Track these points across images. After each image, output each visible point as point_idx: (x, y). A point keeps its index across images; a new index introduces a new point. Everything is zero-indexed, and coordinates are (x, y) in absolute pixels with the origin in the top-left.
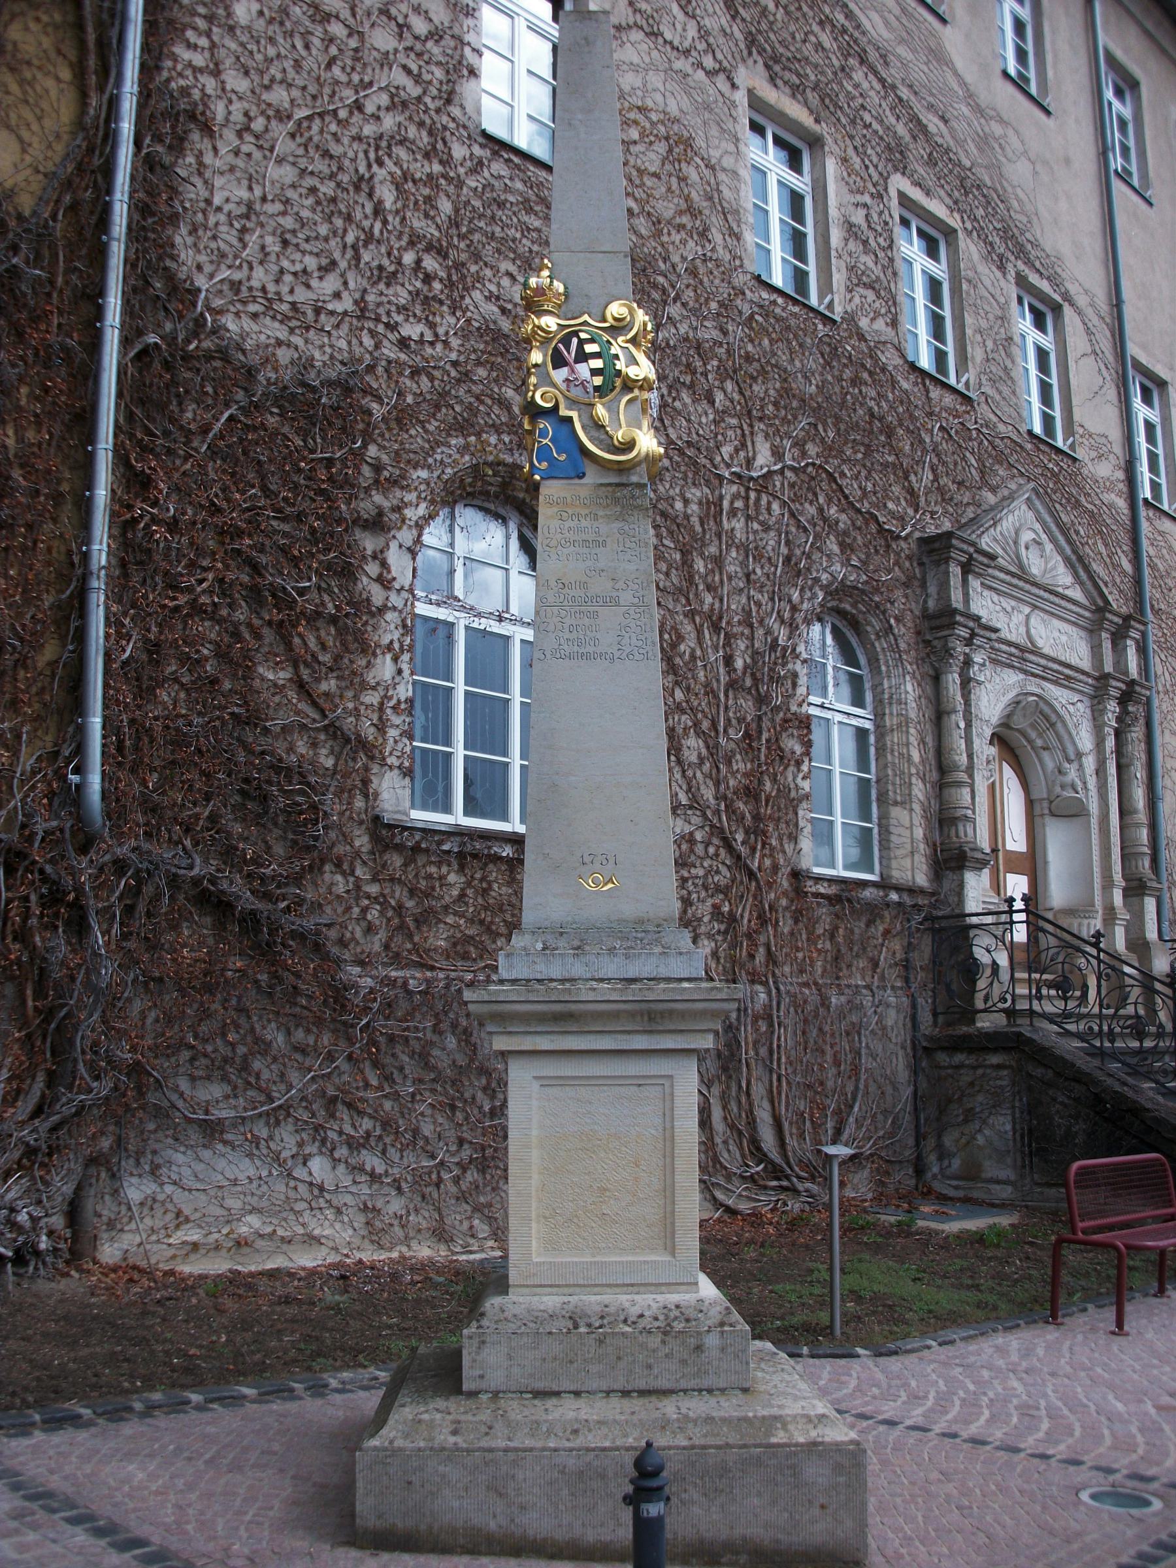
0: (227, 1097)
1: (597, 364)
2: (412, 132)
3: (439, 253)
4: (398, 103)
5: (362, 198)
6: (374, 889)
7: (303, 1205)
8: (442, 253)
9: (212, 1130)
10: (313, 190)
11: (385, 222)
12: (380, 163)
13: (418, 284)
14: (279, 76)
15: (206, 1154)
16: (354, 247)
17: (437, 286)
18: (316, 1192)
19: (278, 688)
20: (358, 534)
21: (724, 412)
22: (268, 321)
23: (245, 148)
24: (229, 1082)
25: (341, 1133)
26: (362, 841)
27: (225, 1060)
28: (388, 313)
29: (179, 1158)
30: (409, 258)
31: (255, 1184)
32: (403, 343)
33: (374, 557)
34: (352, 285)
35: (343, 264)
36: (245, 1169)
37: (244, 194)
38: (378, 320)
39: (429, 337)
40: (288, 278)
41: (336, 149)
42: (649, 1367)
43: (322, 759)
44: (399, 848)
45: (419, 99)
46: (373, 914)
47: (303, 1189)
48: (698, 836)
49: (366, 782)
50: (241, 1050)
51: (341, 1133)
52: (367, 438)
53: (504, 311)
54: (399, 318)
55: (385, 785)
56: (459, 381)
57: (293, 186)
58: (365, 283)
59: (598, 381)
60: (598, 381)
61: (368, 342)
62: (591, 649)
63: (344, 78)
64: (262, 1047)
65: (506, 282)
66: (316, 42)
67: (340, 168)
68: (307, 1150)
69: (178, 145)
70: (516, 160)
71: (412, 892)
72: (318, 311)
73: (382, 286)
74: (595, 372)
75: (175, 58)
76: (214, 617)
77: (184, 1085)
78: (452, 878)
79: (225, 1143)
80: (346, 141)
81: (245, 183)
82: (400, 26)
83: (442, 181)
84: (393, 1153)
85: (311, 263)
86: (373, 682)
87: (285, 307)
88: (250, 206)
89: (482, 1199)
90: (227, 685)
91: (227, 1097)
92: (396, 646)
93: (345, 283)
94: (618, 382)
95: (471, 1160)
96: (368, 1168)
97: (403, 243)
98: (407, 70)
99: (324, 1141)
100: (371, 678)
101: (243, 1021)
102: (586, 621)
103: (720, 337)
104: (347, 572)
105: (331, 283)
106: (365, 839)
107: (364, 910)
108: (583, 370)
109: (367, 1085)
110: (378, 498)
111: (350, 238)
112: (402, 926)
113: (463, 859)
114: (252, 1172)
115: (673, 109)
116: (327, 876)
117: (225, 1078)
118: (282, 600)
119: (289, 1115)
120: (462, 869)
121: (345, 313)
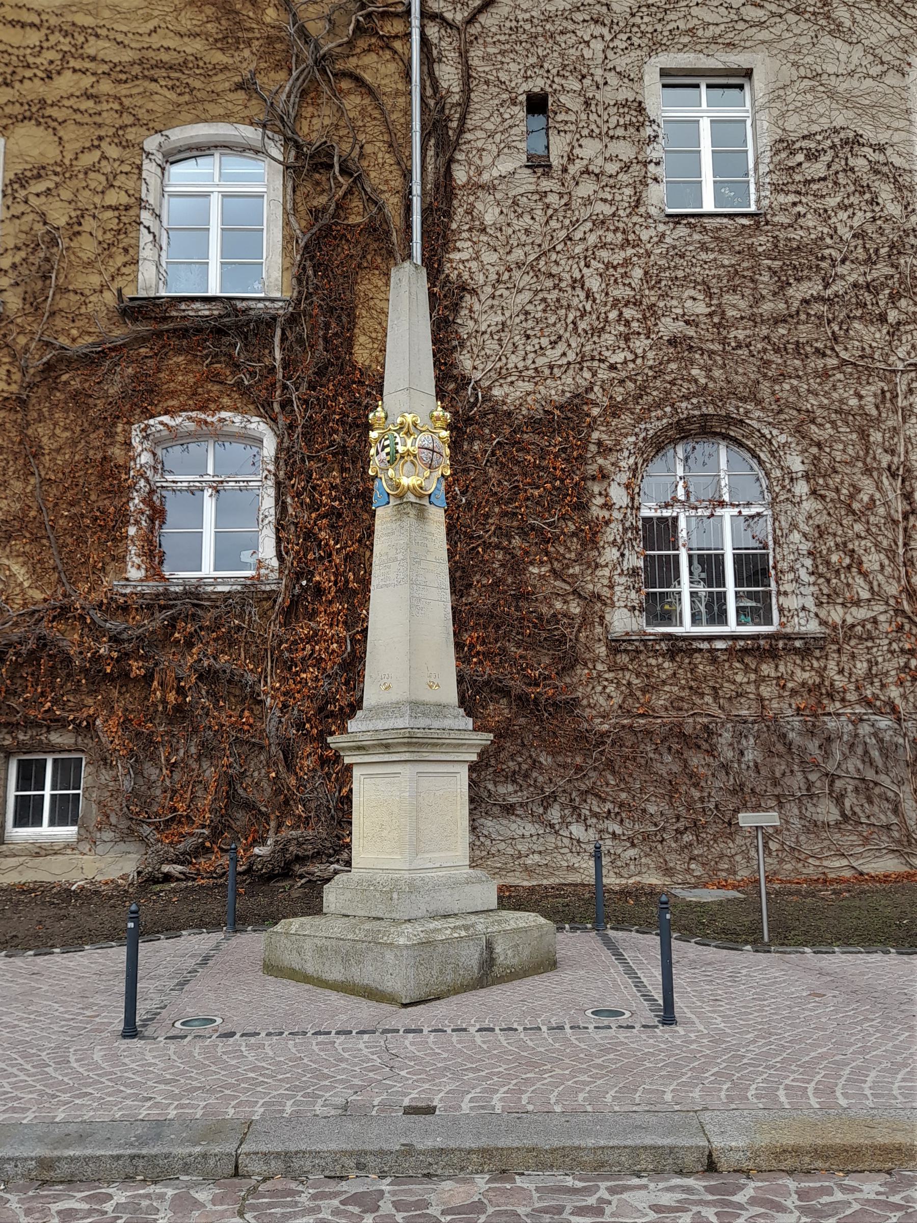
0: (516, 792)
2: (610, 237)
3: (635, 304)
4: (600, 223)
5: (578, 291)
6: (610, 675)
7: (566, 850)
8: (637, 304)
9: (509, 810)
10: (544, 300)
11: (594, 300)
12: (587, 266)
13: (622, 328)
14: (515, 244)
15: (505, 822)
16: (574, 323)
17: (635, 324)
18: (575, 842)
19: (542, 577)
20: (589, 483)
21: (899, 323)
22: (520, 383)
23: (498, 293)
24: (517, 783)
25: (590, 810)
26: (602, 650)
27: (514, 772)
28: (600, 354)
29: (489, 824)
30: (613, 315)
31: (535, 838)
32: (613, 367)
33: (600, 494)
34: (574, 345)
35: (567, 335)
36: (531, 829)
37: (500, 318)
38: (593, 359)
39: (630, 357)
40: (531, 356)
41: (555, 270)
42: (528, 337)
43: (572, 610)
44: (626, 651)
45: (614, 215)
46: (611, 689)
47: (566, 841)
48: (882, 618)
49: (602, 618)
50: (524, 767)
51: (590, 810)
52: (591, 428)
53: (687, 322)
54: (607, 354)
55: (615, 618)
56: (655, 378)
57: (530, 302)
58: (583, 340)
59: (388, 458)
60: (388, 458)
61: (587, 375)
63: (559, 225)
64: (535, 764)
65: (689, 303)
66: (539, 212)
67: (560, 280)
68: (569, 819)
69: (456, 308)
70: (692, 221)
71: (638, 675)
72: (551, 367)
73: (595, 339)
74: (388, 454)
75: (451, 261)
76: (498, 546)
77: (490, 786)
78: (666, 665)
79: (517, 815)
80: (563, 262)
81: (499, 312)
82: (597, 175)
83: (635, 259)
84: (627, 822)
85: (545, 342)
86: (604, 563)
87: (531, 373)
88: (503, 324)
89: (696, 852)
90: (510, 580)
91: (516, 792)
92: (619, 541)
93: (569, 345)
94: (398, 456)
95: (686, 829)
96: (610, 830)
97: (608, 308)
98: (604, 201)
99: (579, 815)
100: (602, 561)
101: (524, 751)
103: (891, 271)
104: (582, 507)
105: (561, 347)
106: (604, 648)
107: (605, 687)
109: (607, 784)
110: (600, 461)
111: (571, 317)
112: (631, 694)
113: (672, 654)
114: (533, 831)
115: (839, 122)
116: (579, 672)
117: (514, 782)
118: (539, 531)
119: (555, 800)
120: (672, 659)
121: (569, 363)
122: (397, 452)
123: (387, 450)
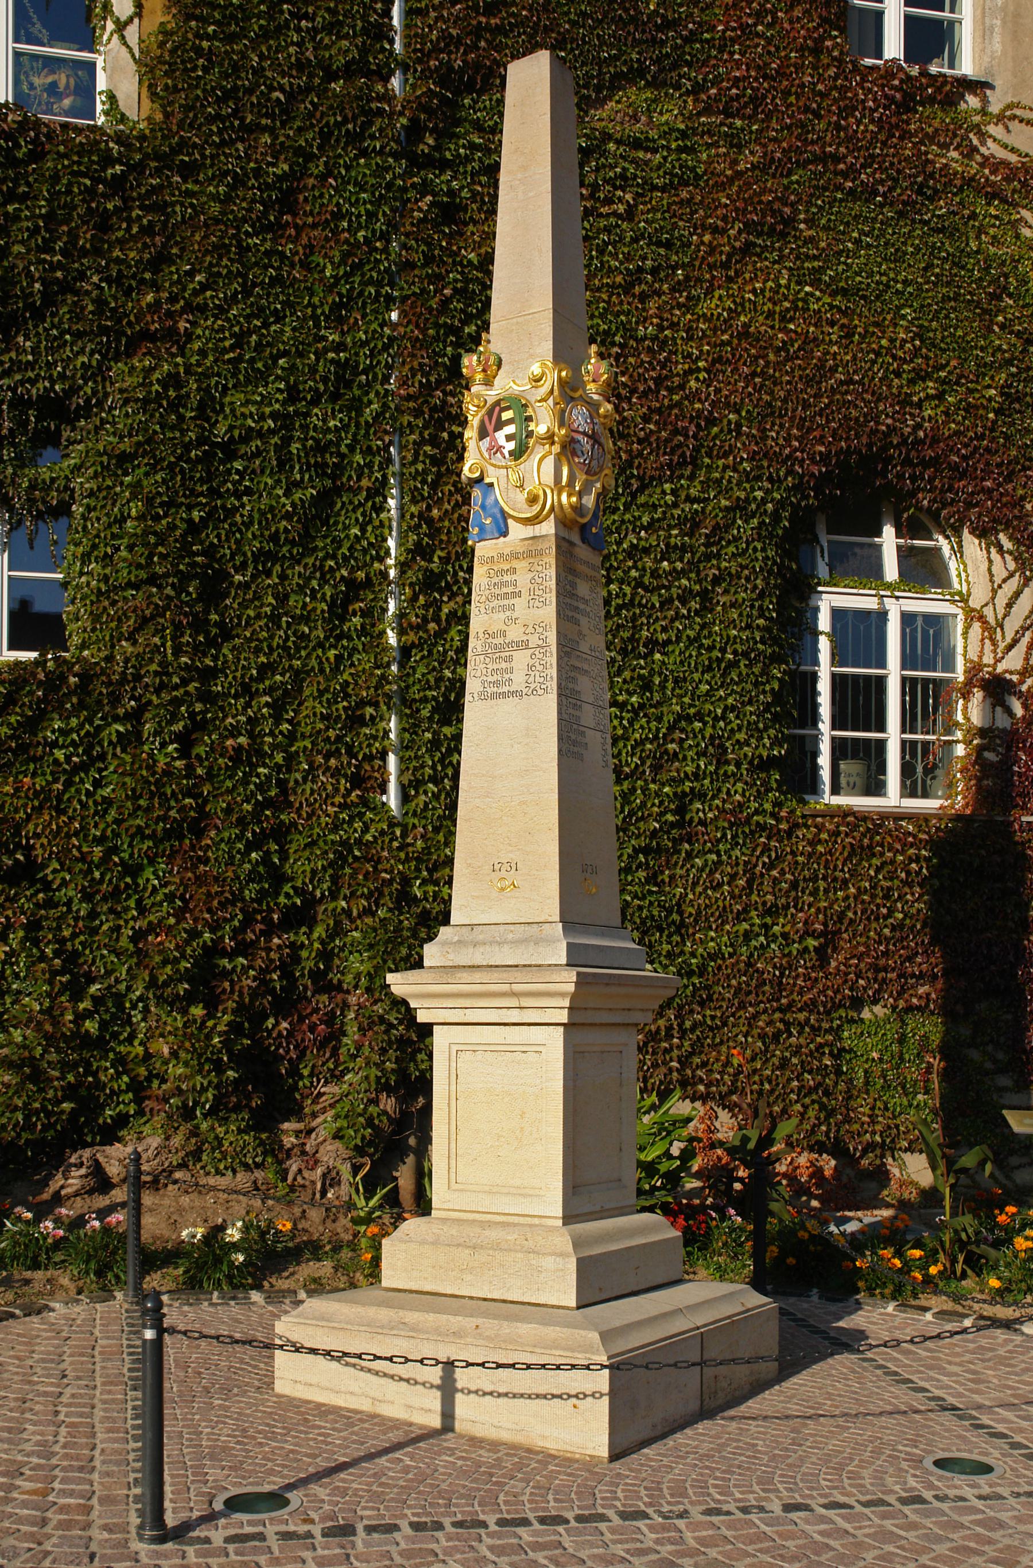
1: (510, 429)
60: (511, 446)
62: (505, 689)
74: (509, 438)
102: (504, 665)
108: (500, 436)
122: (530, 435)
123: (510, 429)
